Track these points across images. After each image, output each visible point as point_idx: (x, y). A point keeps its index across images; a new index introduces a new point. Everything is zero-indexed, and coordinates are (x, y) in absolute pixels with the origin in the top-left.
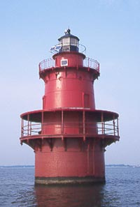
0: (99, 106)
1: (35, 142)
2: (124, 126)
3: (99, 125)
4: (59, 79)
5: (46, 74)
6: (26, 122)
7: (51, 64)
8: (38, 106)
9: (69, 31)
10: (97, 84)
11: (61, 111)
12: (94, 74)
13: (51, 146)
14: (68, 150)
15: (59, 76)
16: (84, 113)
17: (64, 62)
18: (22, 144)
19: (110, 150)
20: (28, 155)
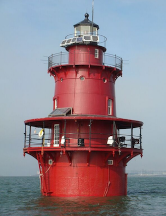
0: (122, 113)
1: (44, 156)
2: (148, 137)
3: (58, 125)
4: (81, 77)
5: (56, 71)
6: (28, 127)
7: (65, 60)
8: (45, 110)
9: (87, 16)
10: (119, 83)
11: (113, 121)
12: (115, 73)
13: (70, 160)
14: (90, 165)
15: (79, 75)
16: (114, 122)
17: (82, 57)
18: (24, 155)
19: (133, 167)
20: (32, 168)
